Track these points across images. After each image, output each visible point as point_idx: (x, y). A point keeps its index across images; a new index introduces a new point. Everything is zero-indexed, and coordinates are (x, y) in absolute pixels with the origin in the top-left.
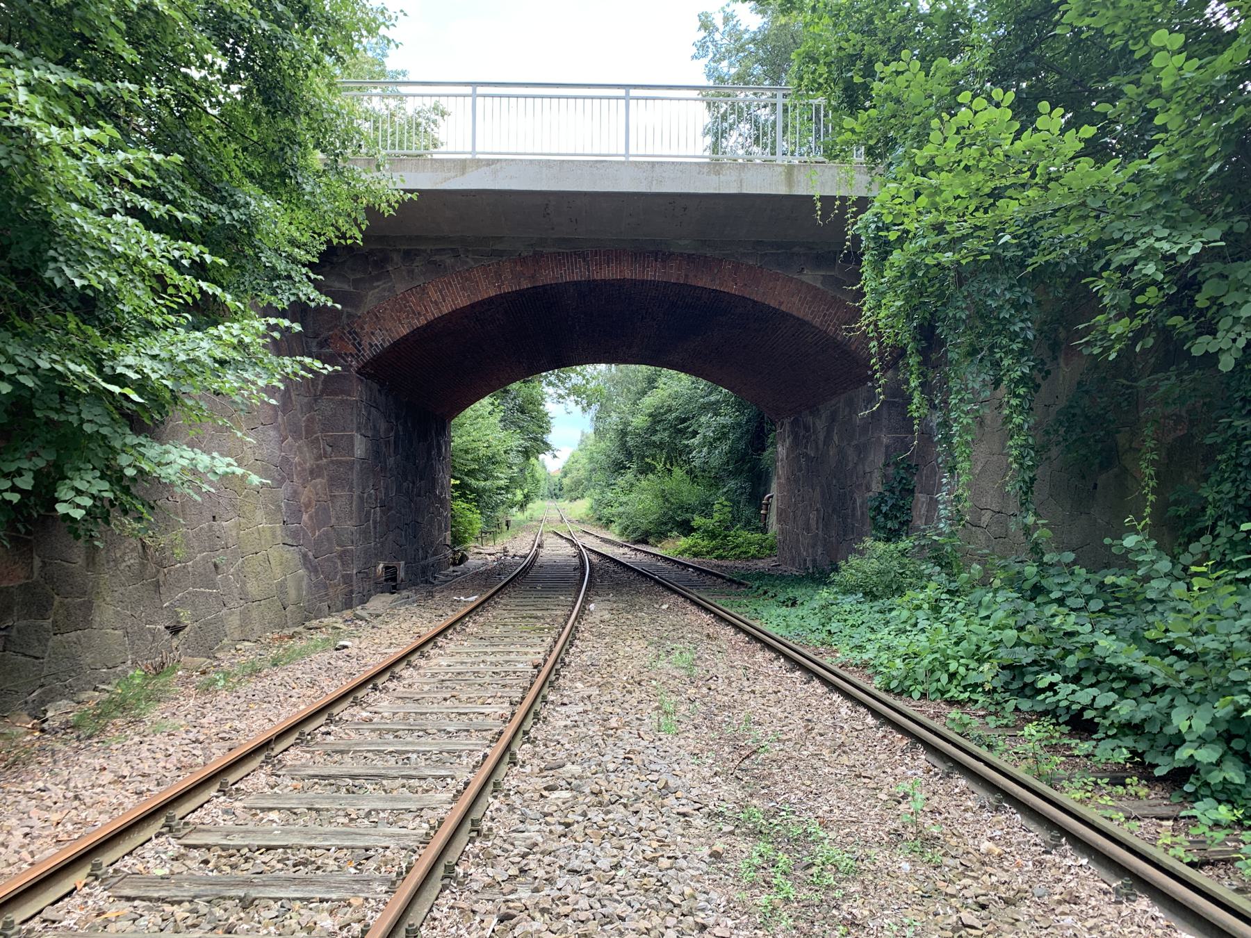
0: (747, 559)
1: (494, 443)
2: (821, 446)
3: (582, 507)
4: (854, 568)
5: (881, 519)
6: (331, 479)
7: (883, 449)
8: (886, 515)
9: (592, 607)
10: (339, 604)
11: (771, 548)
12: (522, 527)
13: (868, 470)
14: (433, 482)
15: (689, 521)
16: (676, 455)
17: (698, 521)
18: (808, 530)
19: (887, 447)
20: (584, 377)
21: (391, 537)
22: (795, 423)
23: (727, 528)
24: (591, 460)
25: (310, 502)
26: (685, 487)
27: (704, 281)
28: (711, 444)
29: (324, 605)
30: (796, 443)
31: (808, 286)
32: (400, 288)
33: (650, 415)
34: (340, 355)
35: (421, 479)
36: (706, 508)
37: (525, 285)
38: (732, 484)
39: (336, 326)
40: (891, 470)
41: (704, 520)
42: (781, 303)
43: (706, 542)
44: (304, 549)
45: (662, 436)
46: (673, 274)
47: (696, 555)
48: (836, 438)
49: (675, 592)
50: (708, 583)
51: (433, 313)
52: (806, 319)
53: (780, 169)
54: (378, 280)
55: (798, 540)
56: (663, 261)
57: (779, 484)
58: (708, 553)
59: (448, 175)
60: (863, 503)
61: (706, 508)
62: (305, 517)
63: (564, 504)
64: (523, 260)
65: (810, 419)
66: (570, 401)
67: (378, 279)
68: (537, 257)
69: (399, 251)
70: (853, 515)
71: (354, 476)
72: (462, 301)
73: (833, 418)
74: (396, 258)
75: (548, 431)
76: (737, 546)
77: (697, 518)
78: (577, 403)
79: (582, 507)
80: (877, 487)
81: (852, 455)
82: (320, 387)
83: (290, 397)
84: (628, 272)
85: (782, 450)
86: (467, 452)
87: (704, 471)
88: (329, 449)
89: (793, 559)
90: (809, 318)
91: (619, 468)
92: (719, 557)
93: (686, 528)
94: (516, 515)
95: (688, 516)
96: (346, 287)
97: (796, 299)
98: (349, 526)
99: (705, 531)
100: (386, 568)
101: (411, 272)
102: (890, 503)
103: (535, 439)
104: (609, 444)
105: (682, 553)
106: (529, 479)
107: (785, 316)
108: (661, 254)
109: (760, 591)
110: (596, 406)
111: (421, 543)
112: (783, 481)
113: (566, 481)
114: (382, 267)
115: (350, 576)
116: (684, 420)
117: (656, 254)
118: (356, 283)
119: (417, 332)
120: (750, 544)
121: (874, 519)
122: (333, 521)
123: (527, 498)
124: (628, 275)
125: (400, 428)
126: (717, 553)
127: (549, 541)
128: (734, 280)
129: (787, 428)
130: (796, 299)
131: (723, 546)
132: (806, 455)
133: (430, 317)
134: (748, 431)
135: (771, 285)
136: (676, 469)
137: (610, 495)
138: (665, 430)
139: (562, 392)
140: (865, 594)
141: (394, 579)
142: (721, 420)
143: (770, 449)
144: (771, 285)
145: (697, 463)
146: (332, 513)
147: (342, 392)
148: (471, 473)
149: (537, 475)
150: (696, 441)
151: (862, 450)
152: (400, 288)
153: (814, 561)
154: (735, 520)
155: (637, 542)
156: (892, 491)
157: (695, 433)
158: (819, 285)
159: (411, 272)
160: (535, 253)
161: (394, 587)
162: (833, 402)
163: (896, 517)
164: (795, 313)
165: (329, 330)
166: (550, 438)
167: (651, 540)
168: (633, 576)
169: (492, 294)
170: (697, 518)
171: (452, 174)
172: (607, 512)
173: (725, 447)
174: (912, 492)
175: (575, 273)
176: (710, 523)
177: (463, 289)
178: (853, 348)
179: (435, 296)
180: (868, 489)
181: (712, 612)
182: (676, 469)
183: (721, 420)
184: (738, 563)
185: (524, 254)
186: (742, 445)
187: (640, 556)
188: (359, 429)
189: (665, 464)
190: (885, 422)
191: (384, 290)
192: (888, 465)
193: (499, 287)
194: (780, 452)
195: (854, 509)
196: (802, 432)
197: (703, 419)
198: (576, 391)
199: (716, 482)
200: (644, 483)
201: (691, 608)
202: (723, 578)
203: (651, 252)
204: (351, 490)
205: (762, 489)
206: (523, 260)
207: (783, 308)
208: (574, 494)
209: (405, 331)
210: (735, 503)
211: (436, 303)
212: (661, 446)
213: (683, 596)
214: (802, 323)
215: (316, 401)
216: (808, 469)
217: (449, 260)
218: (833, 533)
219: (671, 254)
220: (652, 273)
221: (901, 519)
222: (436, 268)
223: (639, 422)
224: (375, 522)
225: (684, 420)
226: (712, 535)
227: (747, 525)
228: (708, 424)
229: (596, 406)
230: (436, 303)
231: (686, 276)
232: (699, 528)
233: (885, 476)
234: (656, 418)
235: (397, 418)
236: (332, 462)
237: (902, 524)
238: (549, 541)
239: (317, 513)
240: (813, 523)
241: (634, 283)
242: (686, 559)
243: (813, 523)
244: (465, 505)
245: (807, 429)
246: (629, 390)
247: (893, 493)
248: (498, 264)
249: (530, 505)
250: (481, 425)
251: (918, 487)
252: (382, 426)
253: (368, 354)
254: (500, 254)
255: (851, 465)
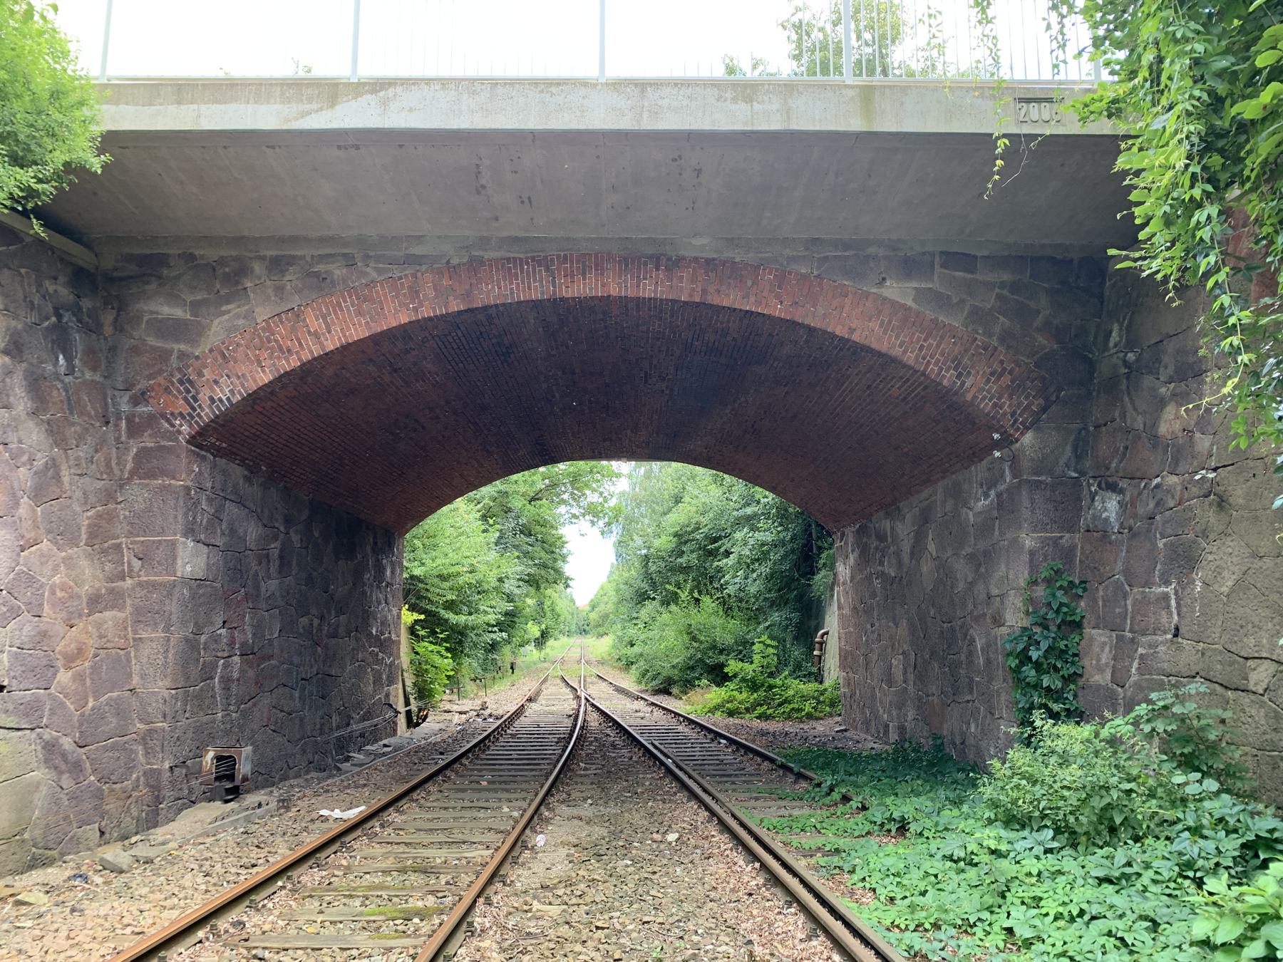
0: (801, 720)
1: (482, 567)
2: (906, 559)
3: (602, 646)
4: (1013, 771)
5: (1029, 672)
6: (138, 611)
7: (1026, 558)
8: (1037, 666)
9: (540, 840)
10: (129, 823)
11: (832, 704)
12: (531, 670)
13: (995, 592)
14: (366, 617)
15: (722, 666)
16: (706, 580)
17: (733, 666)
18: (890, 683)
19: (1032, 553)
20: (601, 494)
21: (266, 700)
22: (862, 531)
23: (771, 675)
24: (617, 591)
25: (80, 651)
26: (718, 621)
27: (731, 298)
28: (748, 565)
29: (92, 831)
30: (865, 557)
31: (894, 304)
32: (263, 313)
33: (676, 535)
34: (163, 416)
35: (340, 612)
36: (743, 649)
37: (456, 306)
38: (776, 617)
39: (160, 372)
40: (1040, 592)
41: (740, 664)
42: (852, 330)
43: (744, 695)
44: (47, 734)
45: (690, 558)
46: (684, 288)
47: (731, 714)
48: (932, 547)
49: (693, 796)
50: (750, 769)
51: (312, 350)
52: (893, 353)
53: (851, 93)
54: (228, 302)
55: (873, 696)
56: (667, 269)
57: (841, 617)
58: (747, 710)
59: (308, 107)
60: (988, 645)
61: (743, 649)
62: (64, 677)
63: (590, 641)
64: (452, 270)
65: (887, 524)
66: (584, 524)
67: (228, 300)
68: (475, 265)
69: (263, 258)
70: (970, 663)
71: (173, 607)
72: (357, 331)
73: (925, 518)
74: (258, 268)
75: (564, 558)
76: (785, 701)
77: (731, 662)
78: (593, 523)
79: (602, 646)
80: (1015, 618)
81: (962, 570)
82: (129, 466)
83: (57, 478)
84: (615, 286)
85: (843, 570)
86: (443, 578)
87: (741, 600)
88: (137, 564)
89: (867, 723)
90: (897, 352)
91: (642, 597)
92: (764, 717)
93: (719, 676)
94: (531, 653)
95: (722, 658)
96: (179, 313)
97: (875, 325)
98: (160, 688)
99: (743, 680)
100: (219, 758)
101: (279, 290)
102: (1044, 645)
103: (545, 566)
104: (634, 573)
105: (713, 710)
106: (549, 614)
107: (857, 351)
108: (665, 261)
109: (836, 796)
110: (616, 529)
111: (337, 703)
112: (846, 611)
113: (593, 616)
114: (237, 283)
115: (159, 772)
116: (715, 540)
117: (657, 260)
118: (195, 306)
119: (283, 380)
120: (805, 698)
121: (1017, 670)
122: (136, 680)
123: (544, 635)
124: (614, 290)
125: (295, 538)
126: (759, 710)
127: (552, 689)
128: (778, 297)
129: (851, 539)
130: (875, 325)
131: (765, 701)
132: (882, 575)
133: (306, 356)
134: (793, 551)
135: (835, 303)
136: (706, 600)
137: (632, 632)
138: (692, 552)
139: (575, 511)
140: (1058, 831)
141: (231, 777)
142: (760, 536)
143: (823, 573)
144: (835, 303)
145: (731, 590)
146: (136, 668)
147: (164, 473)
148: (450, 606)
149: (558, 609)
150: (731, 560)
151: (983, 561)
152: (263, 313)
153: (902, 729)
154: (782, 663)
155: (657, 692)
156: (1044, 625)
157: (728, 554)
158: (910, 303)
159: (279, 290)
160: (472, 260)
161: (228, 791)
162: (924, 495)
163: (1056, 669)
164: (873, 346)
165: (150, 377)
166: (568, 569)
167: (675, 690)
168: (637, 755)
169: (404, 319)
170: (731, 662)
171: (315, 106)
172: (631, 652)
173: (765, 569)
174: (1077, 626)
175: (535, 288)
176: (749, 669)
177: (360, 313)
178: (969, 397)
179: (315, 324)
180: (998, 621)
181: (756, 858)
182: (706, 600)
183: (760, 536)
184: (790, 727)
185: (455, 261)
186: (786, 566)
187: (658, 714)
188: (189, 531)
189: (691, 592)
190: (1026, 514)
191: (238, 316)
192: (1035, 583)
193: (415, 309)
194: (840, 575)
195: (971, 654)
196: (874, 543)
197: (738, 535)
198: (593, 512)
199: (754, 617)
200: (666, 616)
201: (721, 841)
202: (772, 761)
203: (651, 257)
204: (167, 629)
205: (813, 623)
206: (452, 270)
207: (855, 337)
208: (601, 630)
209: (265, 378)
210: (782, 641)
211: (316, 335)
212: (685, 570)
213: (708, 808)
214: (887, 361)
215: (121, 487)
216: (884, 596)
217: (338, 271)
218: (933, 689)
219: (680, 259)
220: (651, 287)
221: (1065, 672)
222: (319, 283)
223: (664, 542)
224: (226, 681)
225: (715, 540)
226: (753, 686)
227: (797, 670)
228: (743, 543)
229: (616, 529)
230: (316, 335)
231: (704, 291)
232: (735, 676)
233: (1031, 601)
234: (682, 537)
235: (288, 521)
236: (140, 584)
237: (1067, 680)
238: (552, 689)
239: (95, 669)
240: (898, 672)
241: (623, 301)
242: (719, 722)
243: (898, 672)
244: (432, 647)
245: (881, 537)
246: (653, 511)
247: (1047, 628)
248: (414, 276)
249: (551, 642)
250: (456, 539)
251: (1089, 620)
252: (252, 532)
253: (207, 414)
254: (418, 260)
255: (961, 586)
